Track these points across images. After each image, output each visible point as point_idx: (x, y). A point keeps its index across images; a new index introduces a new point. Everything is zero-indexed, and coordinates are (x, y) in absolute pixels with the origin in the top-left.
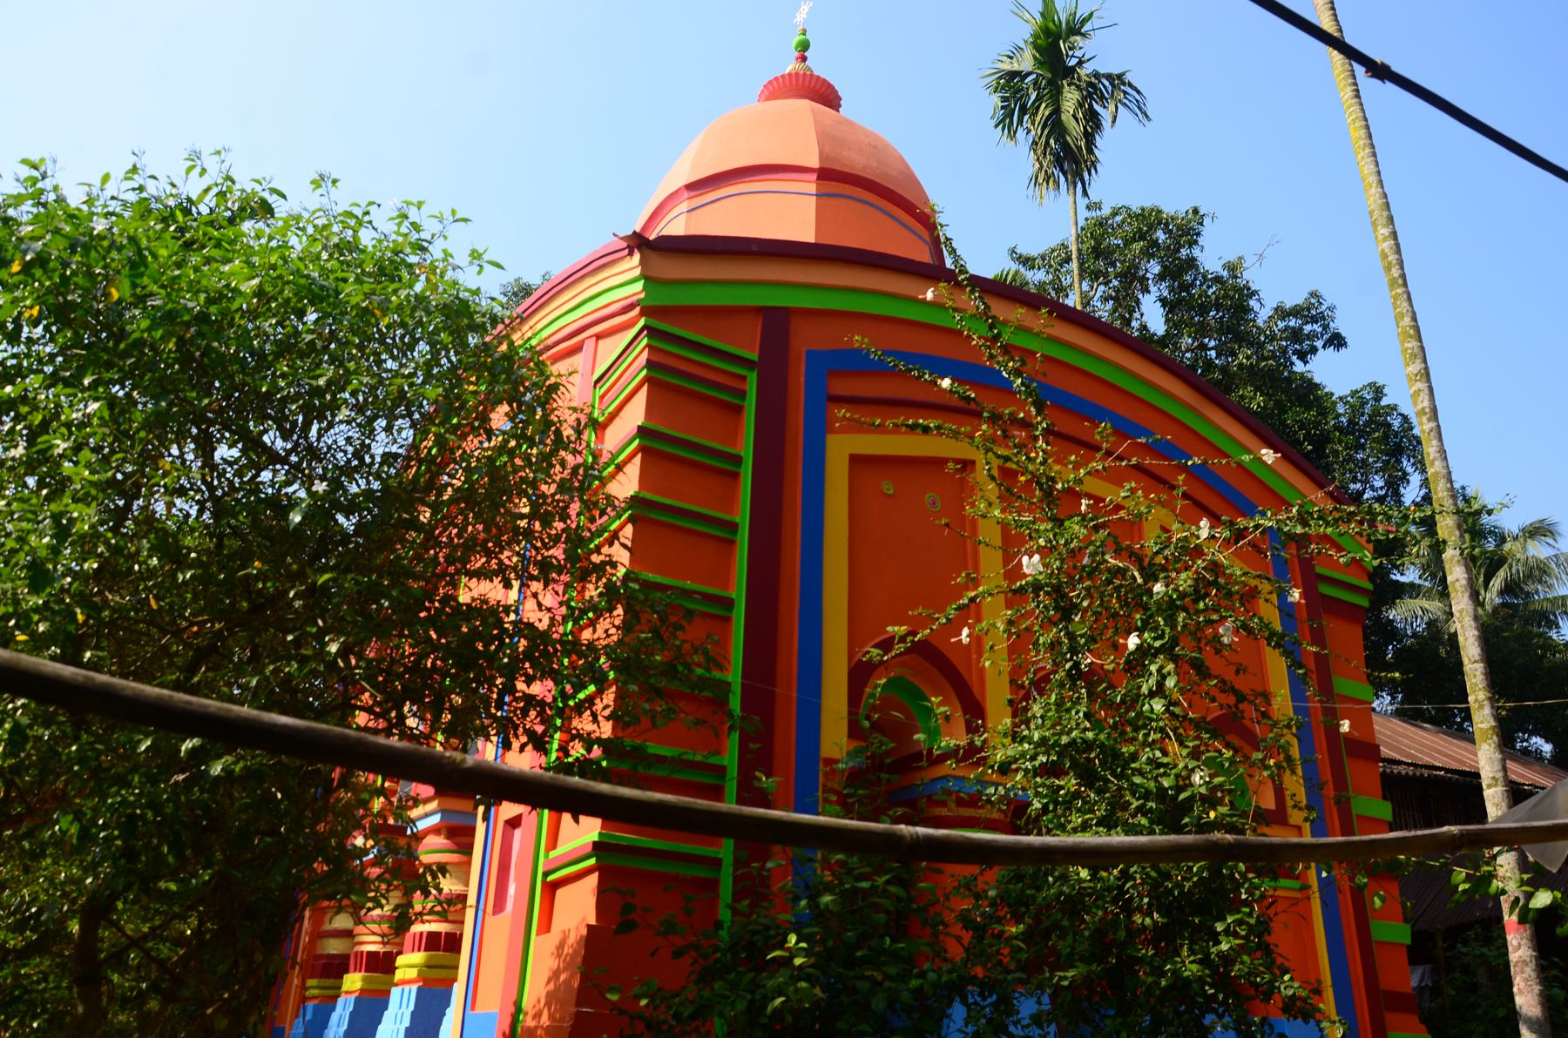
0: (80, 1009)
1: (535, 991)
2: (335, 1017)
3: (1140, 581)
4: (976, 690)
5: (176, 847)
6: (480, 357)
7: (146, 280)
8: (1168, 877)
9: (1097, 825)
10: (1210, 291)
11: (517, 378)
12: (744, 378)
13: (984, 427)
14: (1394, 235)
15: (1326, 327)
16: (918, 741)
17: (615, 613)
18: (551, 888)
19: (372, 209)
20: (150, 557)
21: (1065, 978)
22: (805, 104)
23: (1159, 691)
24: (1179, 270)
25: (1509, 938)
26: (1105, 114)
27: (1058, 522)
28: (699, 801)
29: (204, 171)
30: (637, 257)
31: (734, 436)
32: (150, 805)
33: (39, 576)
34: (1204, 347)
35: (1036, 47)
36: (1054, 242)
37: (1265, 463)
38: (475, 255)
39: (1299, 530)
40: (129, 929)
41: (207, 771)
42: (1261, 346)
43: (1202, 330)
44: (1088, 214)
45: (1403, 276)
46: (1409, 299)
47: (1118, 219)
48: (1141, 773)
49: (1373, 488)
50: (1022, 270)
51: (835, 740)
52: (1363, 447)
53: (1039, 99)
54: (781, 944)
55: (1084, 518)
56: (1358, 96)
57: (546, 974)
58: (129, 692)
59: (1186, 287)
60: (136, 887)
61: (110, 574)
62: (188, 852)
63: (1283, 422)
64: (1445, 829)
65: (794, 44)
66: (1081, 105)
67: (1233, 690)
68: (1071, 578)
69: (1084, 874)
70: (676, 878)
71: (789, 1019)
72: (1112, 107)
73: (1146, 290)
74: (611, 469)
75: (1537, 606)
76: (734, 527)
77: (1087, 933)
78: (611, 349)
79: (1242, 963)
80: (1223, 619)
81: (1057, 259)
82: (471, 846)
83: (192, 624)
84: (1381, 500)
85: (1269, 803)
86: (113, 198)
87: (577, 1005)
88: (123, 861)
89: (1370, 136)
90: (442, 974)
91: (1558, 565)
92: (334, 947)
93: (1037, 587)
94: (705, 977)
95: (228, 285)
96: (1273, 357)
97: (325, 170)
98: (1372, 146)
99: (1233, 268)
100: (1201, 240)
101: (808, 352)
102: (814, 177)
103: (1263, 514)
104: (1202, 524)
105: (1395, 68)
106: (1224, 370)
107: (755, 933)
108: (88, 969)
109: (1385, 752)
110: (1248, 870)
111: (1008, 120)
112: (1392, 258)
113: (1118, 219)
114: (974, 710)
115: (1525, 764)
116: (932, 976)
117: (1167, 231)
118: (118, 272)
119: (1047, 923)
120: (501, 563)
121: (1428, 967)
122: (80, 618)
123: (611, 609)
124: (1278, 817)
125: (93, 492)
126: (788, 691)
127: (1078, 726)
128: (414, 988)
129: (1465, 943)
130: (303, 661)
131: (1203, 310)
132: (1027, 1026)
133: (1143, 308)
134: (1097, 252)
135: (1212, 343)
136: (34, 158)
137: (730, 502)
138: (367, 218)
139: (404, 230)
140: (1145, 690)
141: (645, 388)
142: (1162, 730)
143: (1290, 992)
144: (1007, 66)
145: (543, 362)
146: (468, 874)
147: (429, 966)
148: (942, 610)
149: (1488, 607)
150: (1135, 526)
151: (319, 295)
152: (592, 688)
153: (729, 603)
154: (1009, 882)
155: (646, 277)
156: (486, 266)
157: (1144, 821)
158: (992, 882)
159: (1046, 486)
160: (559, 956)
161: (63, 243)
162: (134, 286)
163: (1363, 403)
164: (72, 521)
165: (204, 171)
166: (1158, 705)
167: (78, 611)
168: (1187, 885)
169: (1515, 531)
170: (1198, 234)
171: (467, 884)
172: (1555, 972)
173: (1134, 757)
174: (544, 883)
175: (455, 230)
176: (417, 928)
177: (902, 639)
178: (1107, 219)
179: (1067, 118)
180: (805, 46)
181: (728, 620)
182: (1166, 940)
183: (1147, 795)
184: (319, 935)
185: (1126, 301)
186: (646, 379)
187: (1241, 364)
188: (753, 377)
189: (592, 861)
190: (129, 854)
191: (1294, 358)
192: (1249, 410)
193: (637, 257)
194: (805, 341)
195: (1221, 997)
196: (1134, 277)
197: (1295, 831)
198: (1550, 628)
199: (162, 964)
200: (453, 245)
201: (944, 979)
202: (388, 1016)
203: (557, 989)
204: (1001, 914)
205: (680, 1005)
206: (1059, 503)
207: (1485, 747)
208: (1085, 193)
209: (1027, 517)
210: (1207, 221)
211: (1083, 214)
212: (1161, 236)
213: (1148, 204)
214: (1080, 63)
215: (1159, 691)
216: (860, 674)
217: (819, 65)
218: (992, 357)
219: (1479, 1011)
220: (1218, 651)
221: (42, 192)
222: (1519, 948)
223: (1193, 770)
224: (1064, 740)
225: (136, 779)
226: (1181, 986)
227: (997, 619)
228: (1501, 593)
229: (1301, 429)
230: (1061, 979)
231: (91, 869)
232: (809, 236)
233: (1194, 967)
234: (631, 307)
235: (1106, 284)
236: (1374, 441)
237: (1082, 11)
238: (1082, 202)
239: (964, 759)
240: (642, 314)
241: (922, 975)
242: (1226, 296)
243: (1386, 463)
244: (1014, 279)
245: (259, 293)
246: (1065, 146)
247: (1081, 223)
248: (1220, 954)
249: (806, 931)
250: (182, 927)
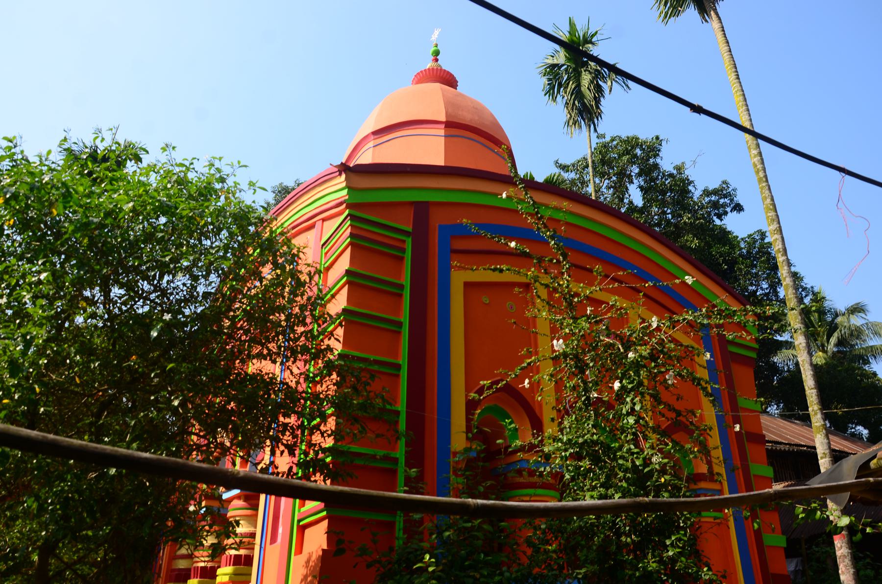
3: (622, 350)
4: (537, 411)
5: (91, 513)
6: (254, 238)
12: (404, 241)
15: (732, 200)
16: (499, 444)
17: (332, 377)
18: (302, 529)
20: (75, 356)
21: (580, 573)
22: (438, 86)
23: (632, 412)
24: (649, 170)
25: (836, 543)
26: (605, 87)
27: (575, 319)
28: (362, 490)
29: (103, 139)
30: (344, 176)
31: (399, 274)
32: (77, 491)
33: (14, 367)
34: (664, 213)
37: (687, 284)
38: (252, 184)
39: (705, 322)
41: (107, 472)
42: (696, 212)
43: (663, 204)
44: (598, 141)
45: (766, 176)
47: (615, 143)
48: (622, 457)
49: (762, 289)
50: (562, 173)
51: (459, 441)
52: (755, 266)
53: (569, 79)
54: (421, 560)
55: (589, 317)
56: (738, 78)
57: (300, 578)
59: (653, 180)
60: (69, 537)
61: (56, 364)
62: (98, 515)
63: (710, 253)
64: (766, 490)
65: (431, 52)
66: (592, 82)
67: (675, 410)
68: (584, 350)
72: (609, 83)
73: (631, 182)
74: (329, 296)
75: (857, 352)
76: (400, 324)
77: (595, 548)
79: (681, 562)
80: (668, 371)
81: (580, 166)
83: (99, 391)
84: (767, 295)
90: (243, 578)
91: (868, 329)
92: (182, 564)
93: (565, 355)
96: (704, 218)
97: (168, 142)
98: (747, 105)
99: (679, 169)
100: (660, 154)
101: (440, 226)
102: (443, 126)
104: (653, 319)
105: (705, 107)
106: (676, 226)
107: (410, 553)
111: (551, 91)
112: (759, 166)
113: (615, 143)
114: (537, 425)
115: (853, 442)
116: (507, 574)
117: (642, 149)
119: (573, 543)
120: (269, 350)
122: (38, 390)
123: (330, 375)
125: (44, 321)
127: (589, 433)
129: (817, 546)
131: (663, 193)
133: (630, 192)
134: (603, 162)
136: (10, 136)
137: (398, 311)
138: (192, 166)
139: (212, 172)
140: (624, 411)
141: (349, 248)
143: (707, 577)
144: (550, 61)
146: (256, 521)
147: (235, 574)
150: (622, 320)
152: (318, 420)
153: (398, 367)
155: (348, 187)
156: (257, 189)
160: (307, 567)
161: (27, 187)
163: (755, 241)
164: (33, 338)
165: (103, 139)
166: (631, 420)
167: (36, 386)
168: (650, 519)
169: (843, 310)
170: (659, 150)
171: (256, 527)
173: (620, 448)
174: (298, 526)
177: (489, 388)
178: (608, 143)
179: (584, 89)
180: (437, 53)
181: (398, 376)
182: (640, 550)
183: (626, 471)
184: (174, 557)
185: (620, 189)
186: (350, 244)
187: (685, 222)
188: (409, 241)
189: (324, 513)
190: (66, 518)
191: (715, 218)
192: (690, 248)
193: (344, 176)
194: (437, 220)
196: (625, 174)
200: (241, 178)
201: (513, 576)
206: (574, 309)
207: (819, 436)
208: (595, 130)
209: (559, 317)
210: (664, 143)
211: (595, 140)
212: (638, 152)
213: (631, 134)
215: (632, 412)
216: (471, 405)
217: (446, 64)
218: (539, 229)
221: (14, 154)
222: (841, 547)
223: (652, 455)
224: (581, 440)
227: (547, 371)
228: (837, 345)
229: (720, 257)
230: (578, 574)
231: (44, 526)
233: (654, 565)
235: (609, 179)
237: (592, 31)
240: (347, 208)
241: (501, 574)
242: (676, 185)
243: (768, 275)
245: (133, 210)
246: (584, 104)
247: (594, 145)
248: (668, 557)
249: (436, 552)
250: (95, 556)
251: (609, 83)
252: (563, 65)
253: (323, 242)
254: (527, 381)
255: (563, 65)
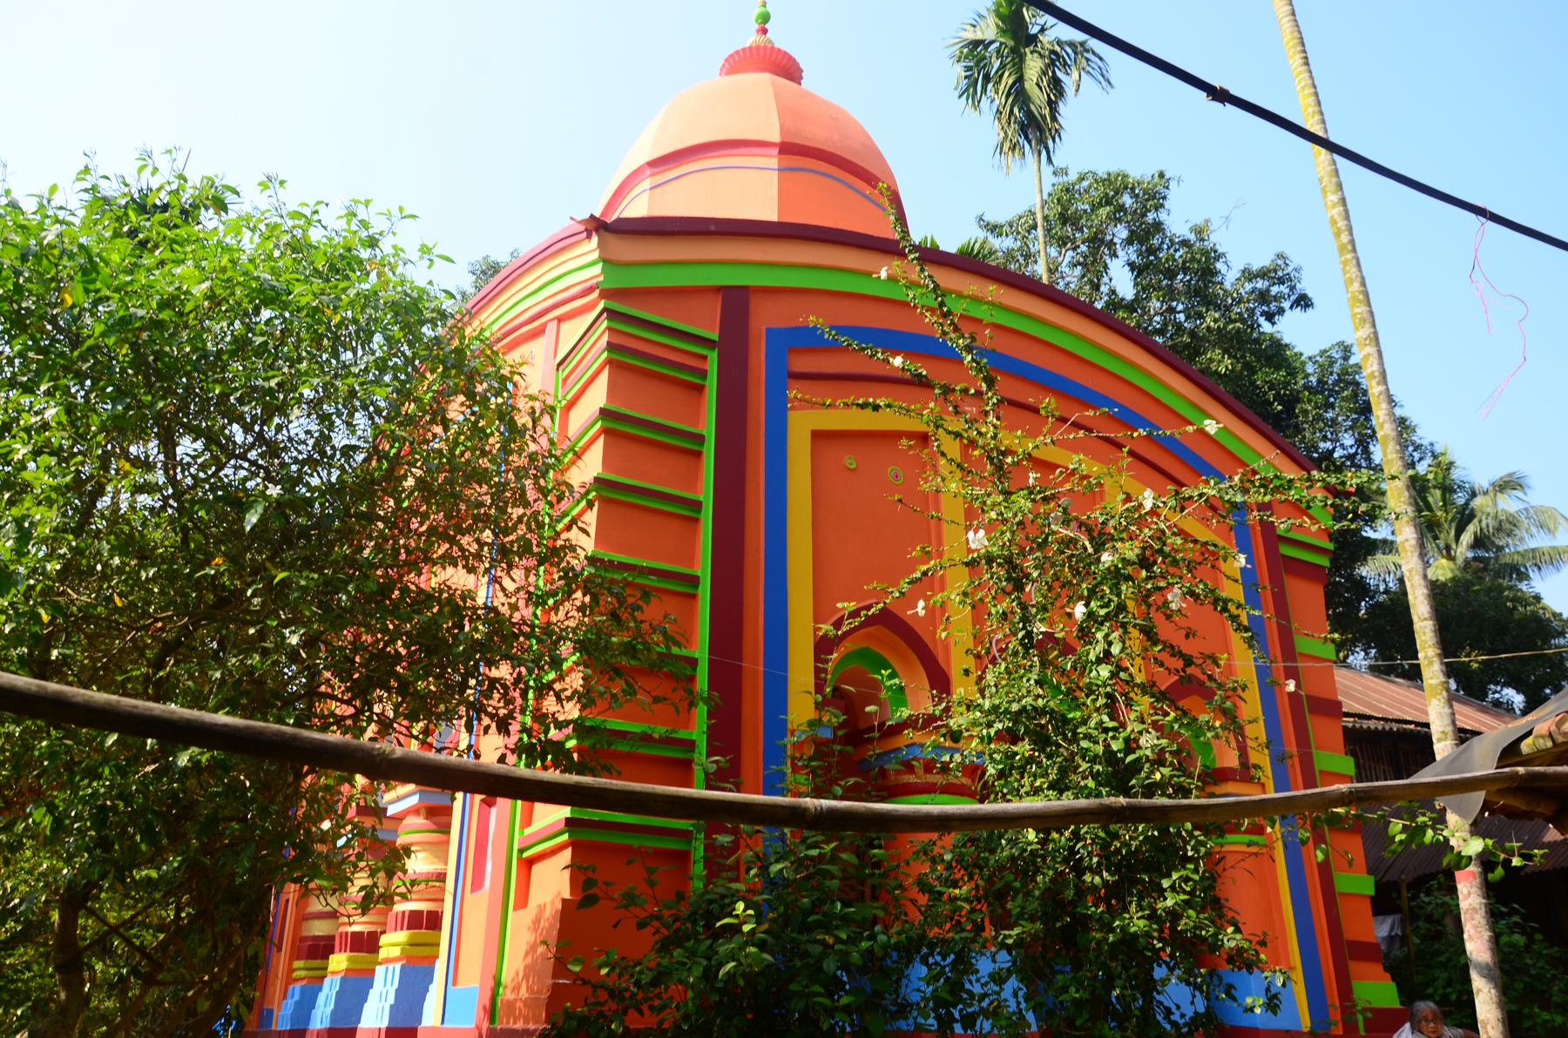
0: (63, 996)
1: (513, 964)
2: (321, 997)
3: (1090, 550)
5: (149, 835)
7: (98, 285)
8: (1116, 836)
9: (1049, 788)
10: (1177, 255)
11: (466, 369)
12: (704, 358)
13: (932, 405)
14: (1343, 201)
15: (1292, 288)
19: (321, 208)
20: (112, 557)
22: (766, 77)
24: (1145, 234)
26: (1068, 82)
27: (1007, 493)
29: (156, 170)
30: (595, 239)
32: (120, 796)
34: (1172, 310)
35: (999, 15)
36: (1021, 209)
38: (425, 250)
39: (1239, 498)
40: (112, 917)
41: (174, 762)
42: (1228, 308)
44: (1055, 180)
45: (1352, 242)
46: (1358, 264)
47: (1085, 184)
48: (1088, 737)
50: (991, 238)
51: (801, 708)
52: (1332, 406)
53: (1002, 67)
56: (1307, 64)
57: (523, 948)
58: (79, 699)
59: (1153, 251)
60: (111, 876)
61: (73, 572)
62: (165, 841)
63: (1253, 383)
64: (1335, 787)
65: (754, 16)
66: (1044, 73)
67: (1181, 655)
68: (1022, 549)
69: (1031, 835)
70: (627, 850)
71: (741, 982)
72: (1075, 75)
73: (1114, 255)
75: (1508, 560)
77: (1037, 893)
78: (572, 331)
80: (1171, 585)
81: (1024, 227)
82: (449, 825)
83: (157, 620)
85: (1232, 760)
86: (61, 208)
87: (554, 976)
88: (98, 851)
89: (1319, 103)
90: (425, 951)
92: (319, 928)
94: (665, 947)
95: (179, 289)
97: (272, 171)
99: (1199, 231)
100: (1167, 204)
101: (769, 330)
102: (776, 151)
103: (1207, 482)
106: (1193, 334)
107: (711, 902)
108: (70, 961)
109: (1349, 705)
110: (1195, 827)
112: (1342, 224)
113: (1085, 184)
114: (940, 682)
116: (882, 938)
118: (72, 278)
119: (999, 885)
121: (1398, 917)
122: (46, 618)
124: (1246, 773)
125: (54, 496)
126: (754, 665)
127: (1030, 693)
128: (398, 966)
129: (1428, 894)
130: (265, 653)
131: (1170, 274)
132: (986, 984)
133: (1111, 272)
134: (1064, 219)
135: (1180, 307)
138: (316, 217)
139: (354, 228)
140: (1092, 657)
141: (606, 370)
142: (1108, 695)
143: (1232, 944)
144: (971, 35)
145: (496, 353)
148: (896, 584)
149: (1460, 561)
150: (1094, 494)
151: (270, 296)
154: (964, 846)
155: (605, 260)
157: (1091, 783)
158: (947, 846)
159: (997, 457)
160: (536, 930)
161: (15, 253)
162: (87, 291)
165: (156, 170)
168: (1134, 843)
169: (1486, 485)
170: (1164, 198)
172: (1516, 919)
174: (520, 859)
175: (403, 227)
176: (401, 907)
177: (854, 614)
178: (1073, 185)
179: (1030, 86)
180: (765, 18)
182: (1116, 896)
183: (1094, 759)
185: (1093, 267)
187: (1208, 328)
188: (713, 356)
189: (565, 837)
190: (104, 843)
193: (595, 239)
194: (764, 318)
195: (1168, 950)
196: (1102, 241)
197: (1259, 788)
198: (1521, 580)
199: (142, 949)
200: (402, 239)
202: (373, 994)
203: (534, 962)
204: (958, 876)
205: (640, 972)
207: (1435, 702)
208: (1049, 159)
210: (1172, 185)
211: (1049, 180)
212: (1127, 200)
213: (1114, 169)
214: (1043, 30)
215: (1106, 657)
216: (823, 646)
217: (780, 37)
218: (944, 333)
219: (1442, 959)
220: (1168, 617)
222: (1469, 896)
223: (1140, 733)
224: (1015, 707)
225: (107, 771)
226: (1129, 941)
230: (1006, 937)
232: (770, 214)
233: (1142, 923)
234: (591, 290)
236: (1343, 399)
238: (1047, 170)
239: (923, 728)
241: (872, 937)
242: (1193, 260)
243: (1355, 421)
244: (982, 247)
245: (211, 296)
246: (1029, 114)
247: (1047, 188)
248: (1168, 911)
251: (1075, 75)
252: (992, 42)
253: (558, 359)
254: (921, 604)
255: (992, 42)
